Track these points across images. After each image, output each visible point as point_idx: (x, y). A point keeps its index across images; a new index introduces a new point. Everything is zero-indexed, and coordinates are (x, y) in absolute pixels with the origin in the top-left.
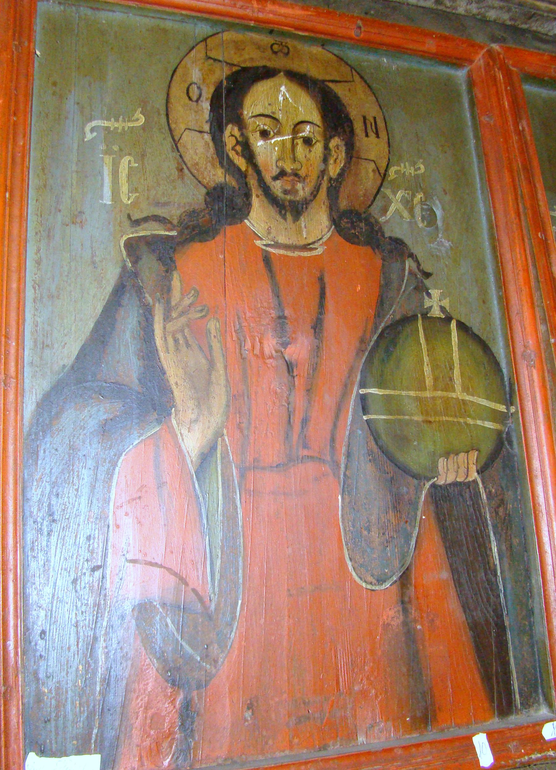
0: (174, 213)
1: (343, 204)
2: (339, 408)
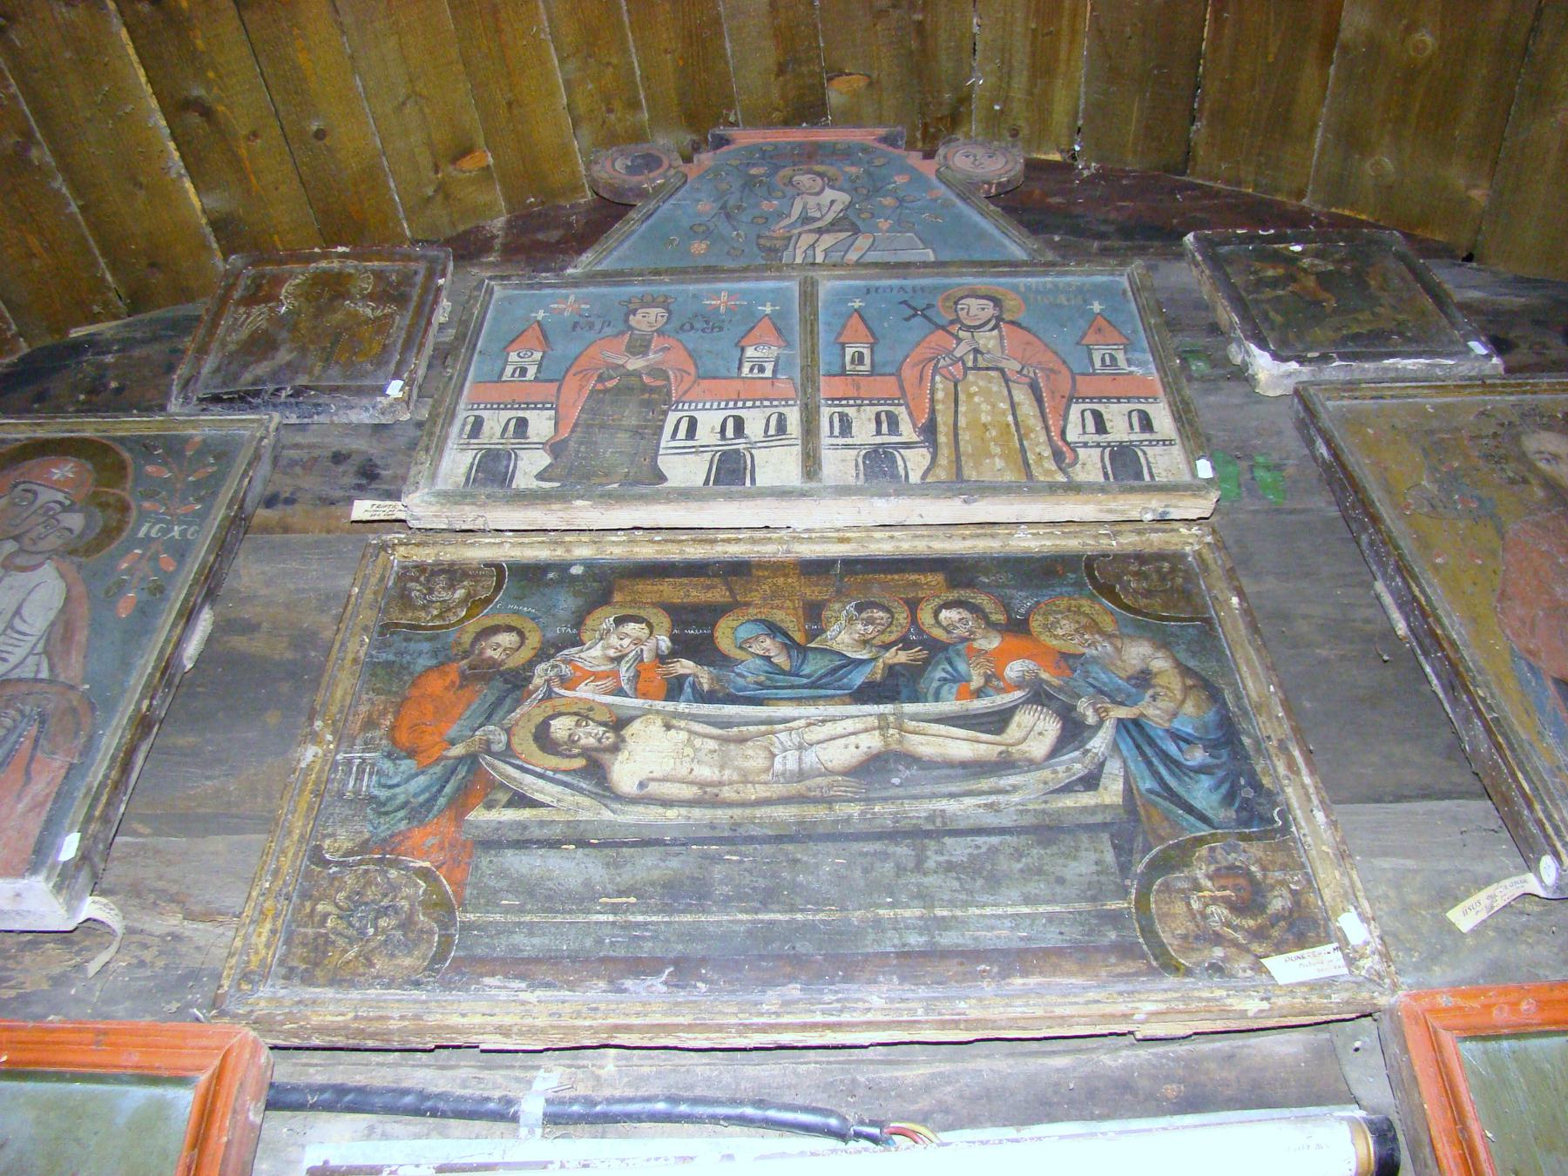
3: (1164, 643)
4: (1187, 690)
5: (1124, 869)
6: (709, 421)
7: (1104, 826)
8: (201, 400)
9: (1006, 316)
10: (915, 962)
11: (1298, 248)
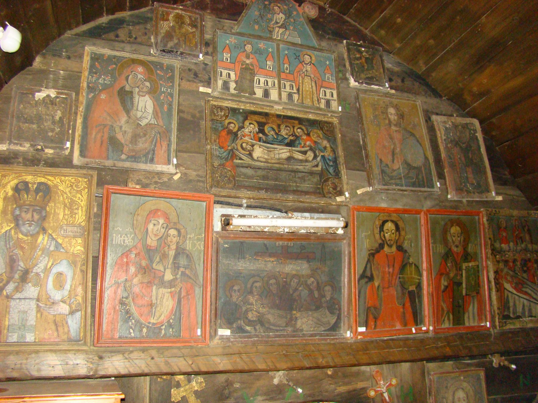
0: (374, 248)
1: (398, 244)
2: (396, 279)
3: (329, 141)
4: (331, 151)
5: (321, 180)
6: (262, 80)
7: (318, 174)
8: (161, 51)
9: (312, 62)
10: (295, 192)
11: (363, 49)
